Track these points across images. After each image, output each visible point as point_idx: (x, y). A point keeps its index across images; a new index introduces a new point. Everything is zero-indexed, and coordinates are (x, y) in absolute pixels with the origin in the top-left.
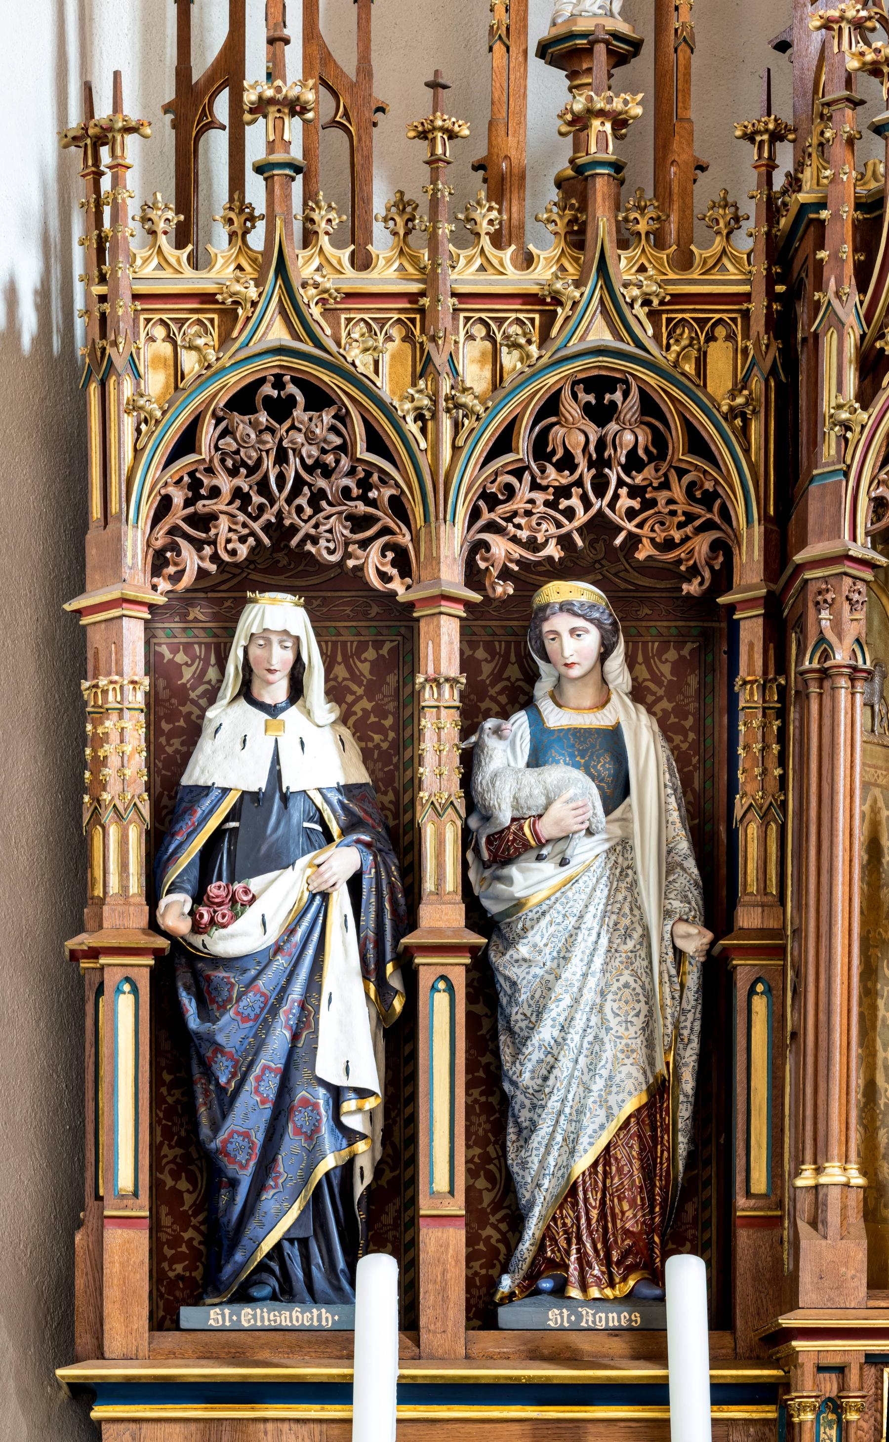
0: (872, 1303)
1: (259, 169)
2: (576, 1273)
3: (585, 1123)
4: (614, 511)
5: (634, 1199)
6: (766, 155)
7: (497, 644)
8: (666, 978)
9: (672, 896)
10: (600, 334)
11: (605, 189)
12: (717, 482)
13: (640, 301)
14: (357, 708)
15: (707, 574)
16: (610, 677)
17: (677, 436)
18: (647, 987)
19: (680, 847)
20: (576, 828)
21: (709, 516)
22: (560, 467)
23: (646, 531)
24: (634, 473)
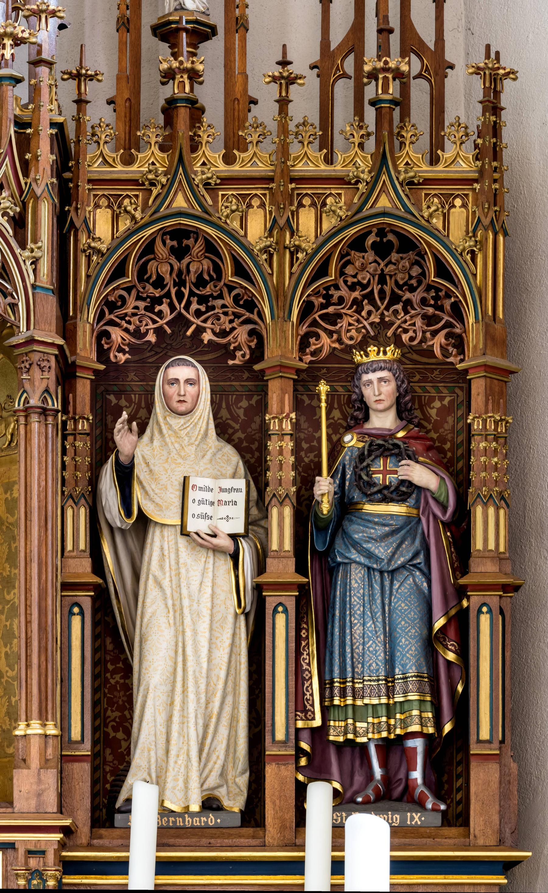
1: (373, 103)
7: (133, 396)
17: (228, 268)
23: (208, 325)
24: (201, 288)
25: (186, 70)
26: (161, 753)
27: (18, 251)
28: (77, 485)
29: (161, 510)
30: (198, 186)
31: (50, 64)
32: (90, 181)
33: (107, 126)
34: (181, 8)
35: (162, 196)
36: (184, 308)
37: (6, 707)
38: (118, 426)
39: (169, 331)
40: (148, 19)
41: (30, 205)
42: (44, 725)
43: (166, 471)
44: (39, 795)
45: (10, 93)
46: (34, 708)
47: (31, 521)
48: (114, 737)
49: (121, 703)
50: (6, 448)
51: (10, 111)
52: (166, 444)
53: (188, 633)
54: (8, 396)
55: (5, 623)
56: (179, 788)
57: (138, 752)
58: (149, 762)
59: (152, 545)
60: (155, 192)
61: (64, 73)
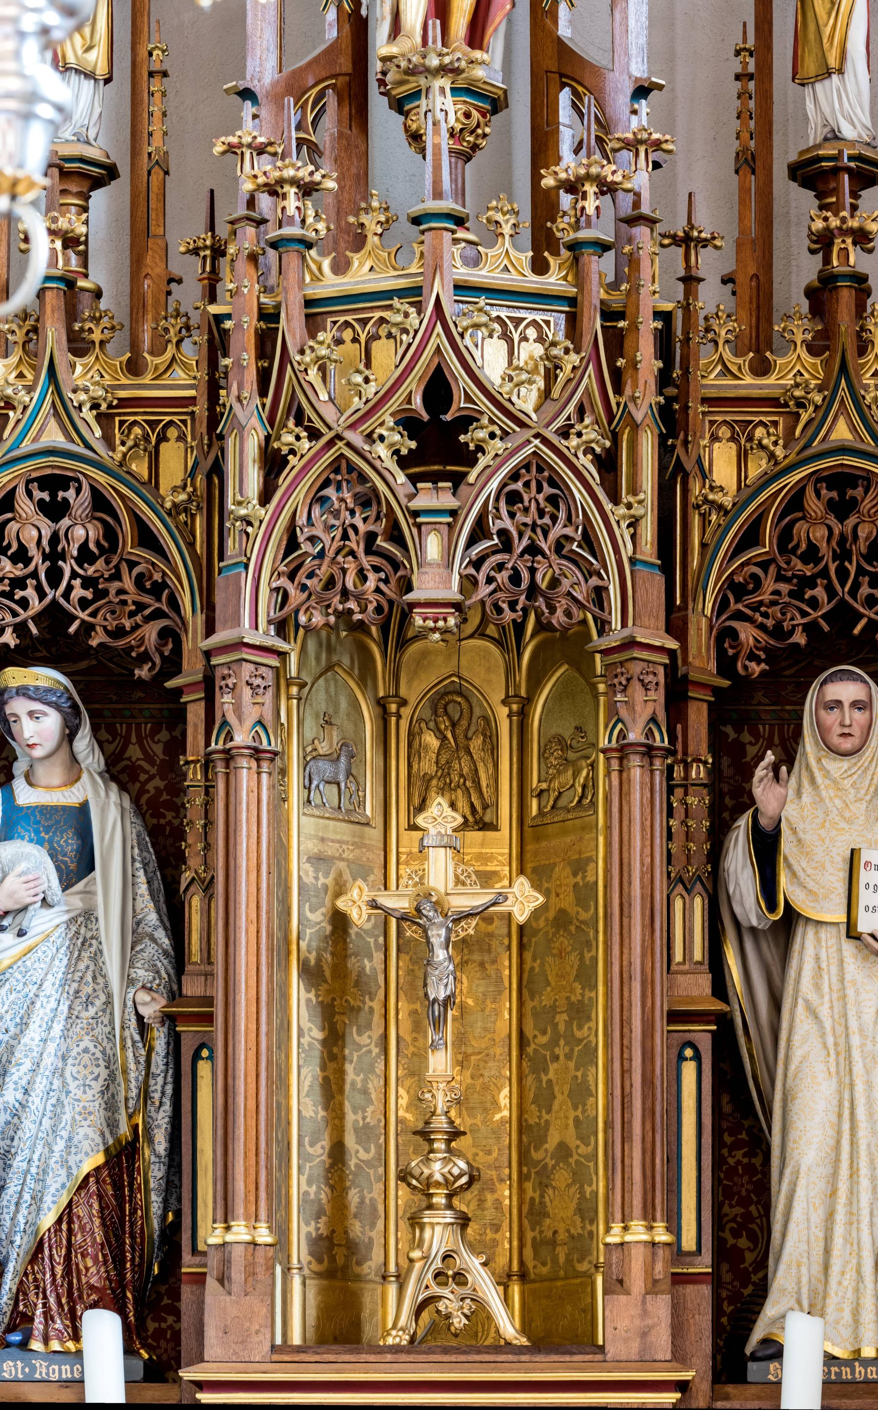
0: (275, 1357)
2: (41, 1327)
3: (49, 1182)
4: (68, 601)
5: (97, 1256)
6: (208, 269)
8: (129, 1043)
9: (139, 965)
10: (54, 436)
11: (54, 302)
12: (164, 574)
13: (88, 405)
14: (150, 787)
15: (158, 660)
16: (80, 757)
18: (108, 1051)
19: (149, 918)
20: (29, 900)
21: (157, 605)
22: (14, 560)
25: (851, 231)
26: (817, 1268)
27: (608, 506)
28: (689, 863)
29: (816, 900)
30: (869, 407)
31: (651, 222)
32: (705, 401)
33: (729, 316)
34: (834, 136)
35: (816, 423)
36: (849, 593)
37: (575, 1201)
38: (759, 772)
39: (826, 628)
40: (785, 152)
41: (625, 437)
42: (650, 1228)
43: (823, 840)
44: (644, 1334)
45: (594, 267)
46: (635, 1202)
47: (630, 917)
48: (734, 1246)
49: (744, 1193)
50: (574, 808)
51: (594, 294)
52: (822, 800)
53: (860, 1088)
54: (577, 728)
55: (574, 1073)
56: (844, 1322)
57: (782, 1267)
58: (799, 1282)
59: (801, 953)
60: (804, 417)
61: (664, 236)
